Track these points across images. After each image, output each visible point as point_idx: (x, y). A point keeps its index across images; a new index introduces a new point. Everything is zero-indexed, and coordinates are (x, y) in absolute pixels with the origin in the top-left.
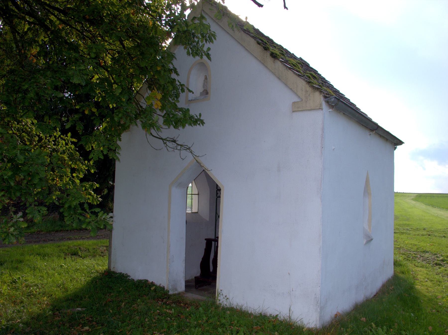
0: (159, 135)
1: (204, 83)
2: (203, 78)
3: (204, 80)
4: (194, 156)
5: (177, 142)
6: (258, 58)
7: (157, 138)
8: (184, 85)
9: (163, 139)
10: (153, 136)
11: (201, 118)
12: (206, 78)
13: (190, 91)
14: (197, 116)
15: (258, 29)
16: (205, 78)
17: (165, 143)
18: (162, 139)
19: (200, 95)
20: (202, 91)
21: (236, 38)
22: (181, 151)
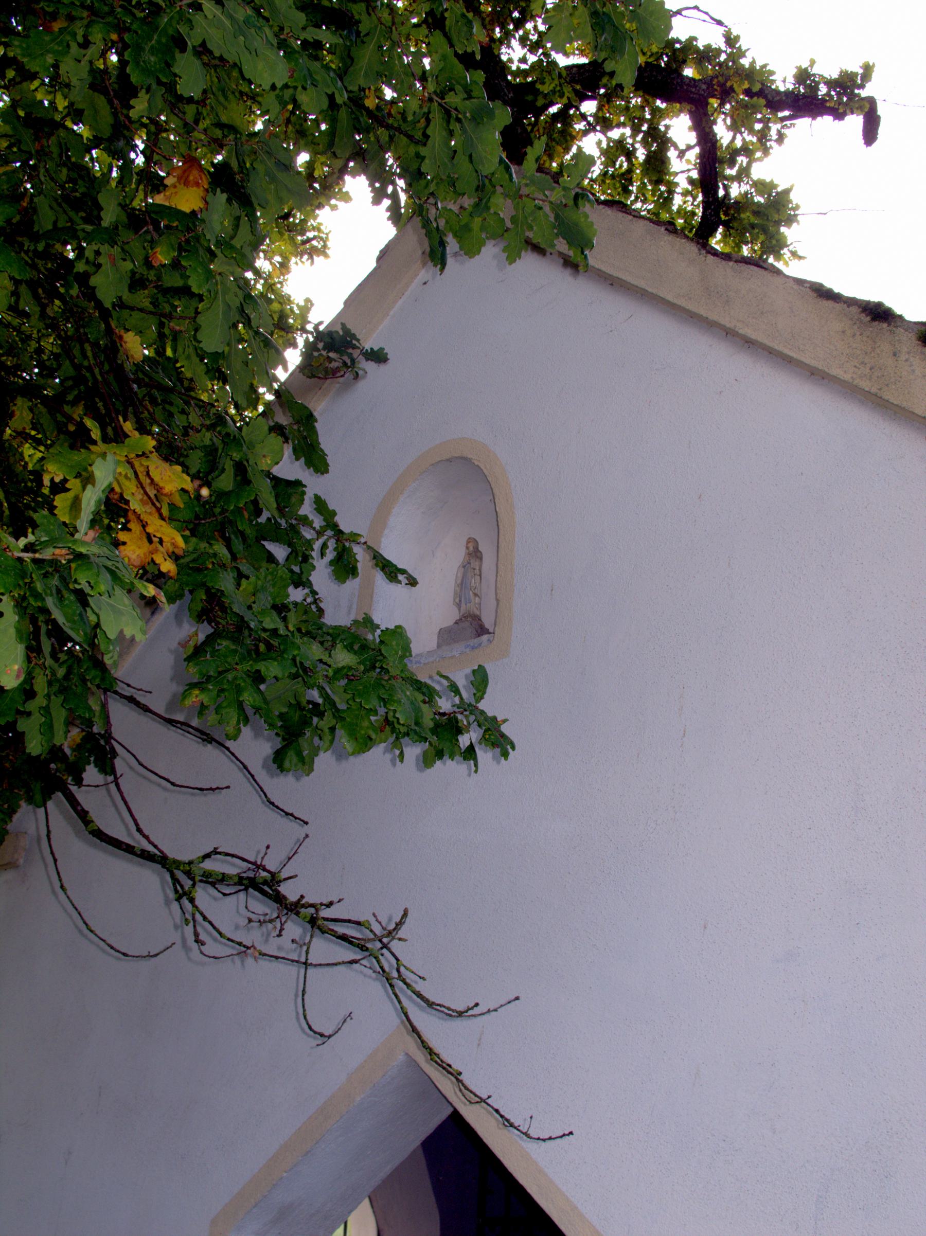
0: (147, 838)
1: (464, 576)
2: (459, 555)
3: (465, 566)
4: (462, 1088)
5: (290, 891)
6: (835, 371)
7: (129, 849)
8: (354, 537)
9: (177, 863)
10: (100, 835)
11: (488, 705)
12: (474, 553)
13: (391, 571)
14: (455, 689)
15: (877, 141)
16: (469, 554)
17: (183, 895)
18: (162, 860)
19: (439, 646)
20: (449, 622)
21: (670, 298)
22: (310, 971)
